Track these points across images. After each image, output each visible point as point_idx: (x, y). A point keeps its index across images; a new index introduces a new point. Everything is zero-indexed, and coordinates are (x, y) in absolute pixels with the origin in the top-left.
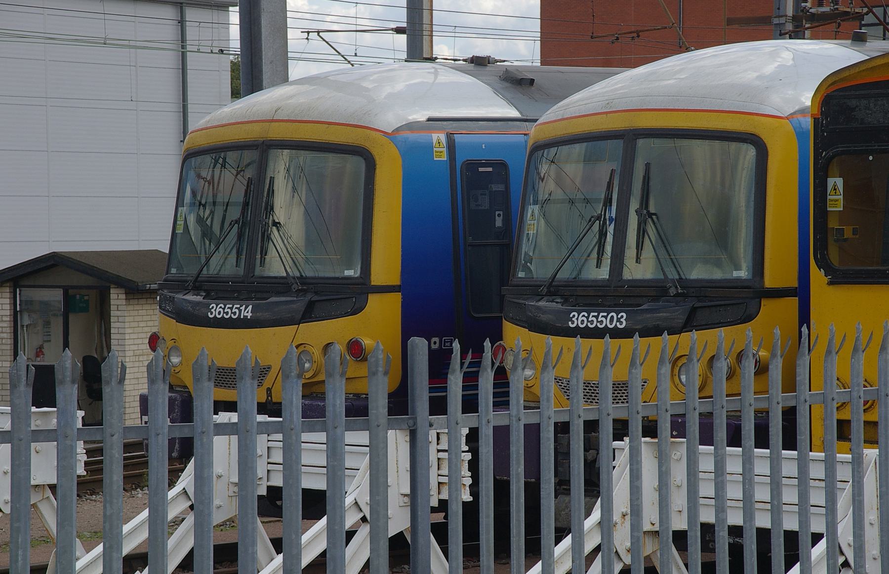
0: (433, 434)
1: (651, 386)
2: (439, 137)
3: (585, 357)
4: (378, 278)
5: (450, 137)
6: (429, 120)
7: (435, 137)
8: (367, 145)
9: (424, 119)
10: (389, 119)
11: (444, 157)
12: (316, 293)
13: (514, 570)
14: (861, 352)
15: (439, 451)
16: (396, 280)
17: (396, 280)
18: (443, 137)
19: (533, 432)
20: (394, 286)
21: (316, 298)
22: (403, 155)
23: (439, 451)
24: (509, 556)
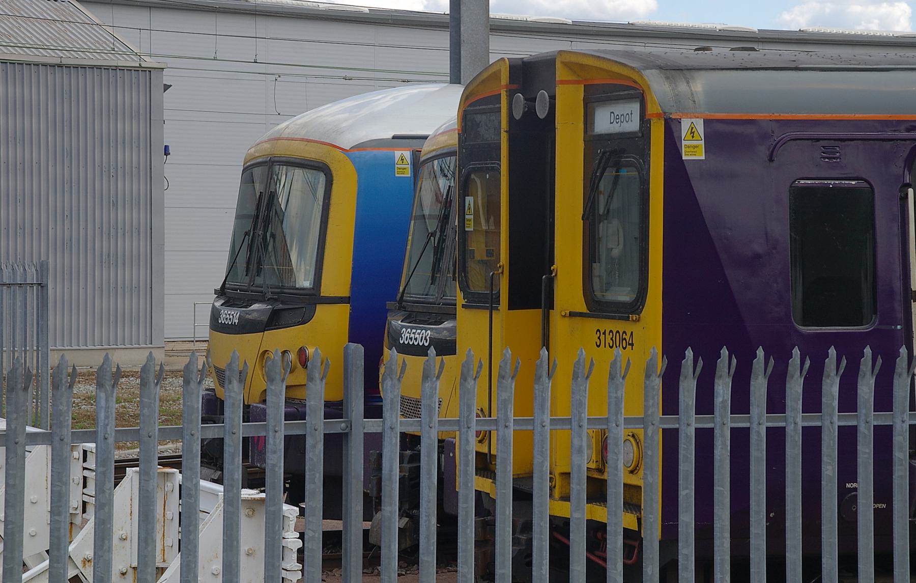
0: (78, 454)
1: (444, 404)
2: (403, 155)
3: (587, 367)
4: (327, 290)
5: (416, 154)
6: (394, 137)
7: (398, 154)
8: (328, 161)
9: (390, 137)
10: (348, 141)
11: (408, 174)
12: (282, 303)
13: (384, 576)
14: (21, 393)
15: (84, 469)
16: (345, 292)
17: (345, 292)
18: (407, 154)
19: (410, 442)
20: (341, 298)
21: (281, 306)
22: (359, 171)
23: (84, 469)
24: (455, 559)
